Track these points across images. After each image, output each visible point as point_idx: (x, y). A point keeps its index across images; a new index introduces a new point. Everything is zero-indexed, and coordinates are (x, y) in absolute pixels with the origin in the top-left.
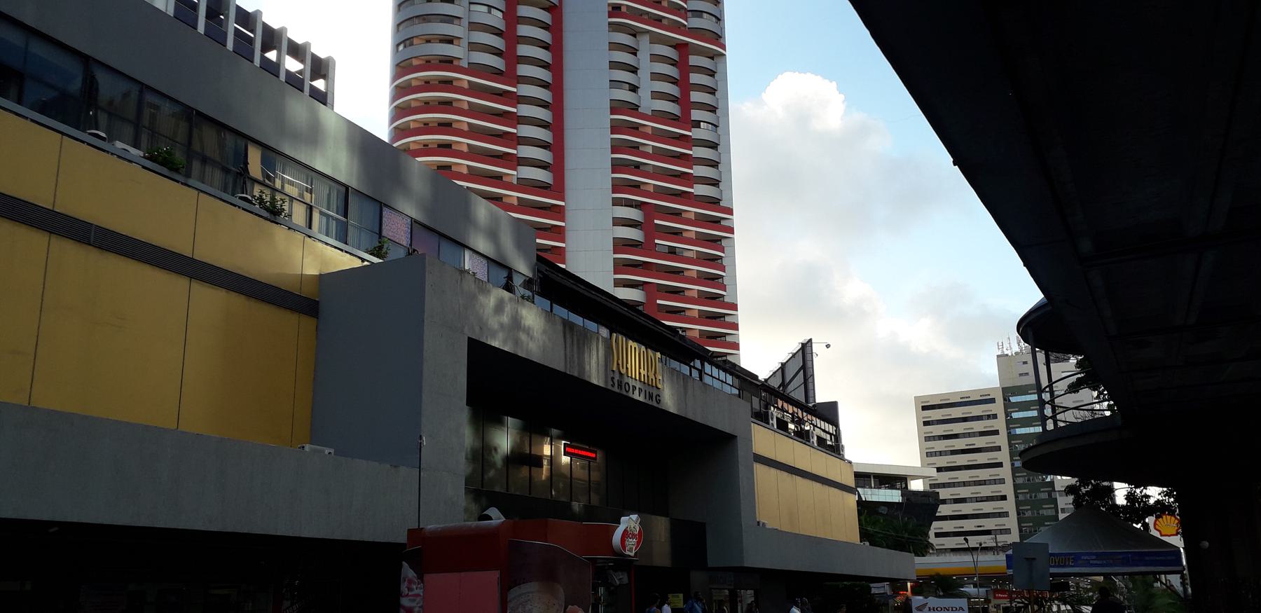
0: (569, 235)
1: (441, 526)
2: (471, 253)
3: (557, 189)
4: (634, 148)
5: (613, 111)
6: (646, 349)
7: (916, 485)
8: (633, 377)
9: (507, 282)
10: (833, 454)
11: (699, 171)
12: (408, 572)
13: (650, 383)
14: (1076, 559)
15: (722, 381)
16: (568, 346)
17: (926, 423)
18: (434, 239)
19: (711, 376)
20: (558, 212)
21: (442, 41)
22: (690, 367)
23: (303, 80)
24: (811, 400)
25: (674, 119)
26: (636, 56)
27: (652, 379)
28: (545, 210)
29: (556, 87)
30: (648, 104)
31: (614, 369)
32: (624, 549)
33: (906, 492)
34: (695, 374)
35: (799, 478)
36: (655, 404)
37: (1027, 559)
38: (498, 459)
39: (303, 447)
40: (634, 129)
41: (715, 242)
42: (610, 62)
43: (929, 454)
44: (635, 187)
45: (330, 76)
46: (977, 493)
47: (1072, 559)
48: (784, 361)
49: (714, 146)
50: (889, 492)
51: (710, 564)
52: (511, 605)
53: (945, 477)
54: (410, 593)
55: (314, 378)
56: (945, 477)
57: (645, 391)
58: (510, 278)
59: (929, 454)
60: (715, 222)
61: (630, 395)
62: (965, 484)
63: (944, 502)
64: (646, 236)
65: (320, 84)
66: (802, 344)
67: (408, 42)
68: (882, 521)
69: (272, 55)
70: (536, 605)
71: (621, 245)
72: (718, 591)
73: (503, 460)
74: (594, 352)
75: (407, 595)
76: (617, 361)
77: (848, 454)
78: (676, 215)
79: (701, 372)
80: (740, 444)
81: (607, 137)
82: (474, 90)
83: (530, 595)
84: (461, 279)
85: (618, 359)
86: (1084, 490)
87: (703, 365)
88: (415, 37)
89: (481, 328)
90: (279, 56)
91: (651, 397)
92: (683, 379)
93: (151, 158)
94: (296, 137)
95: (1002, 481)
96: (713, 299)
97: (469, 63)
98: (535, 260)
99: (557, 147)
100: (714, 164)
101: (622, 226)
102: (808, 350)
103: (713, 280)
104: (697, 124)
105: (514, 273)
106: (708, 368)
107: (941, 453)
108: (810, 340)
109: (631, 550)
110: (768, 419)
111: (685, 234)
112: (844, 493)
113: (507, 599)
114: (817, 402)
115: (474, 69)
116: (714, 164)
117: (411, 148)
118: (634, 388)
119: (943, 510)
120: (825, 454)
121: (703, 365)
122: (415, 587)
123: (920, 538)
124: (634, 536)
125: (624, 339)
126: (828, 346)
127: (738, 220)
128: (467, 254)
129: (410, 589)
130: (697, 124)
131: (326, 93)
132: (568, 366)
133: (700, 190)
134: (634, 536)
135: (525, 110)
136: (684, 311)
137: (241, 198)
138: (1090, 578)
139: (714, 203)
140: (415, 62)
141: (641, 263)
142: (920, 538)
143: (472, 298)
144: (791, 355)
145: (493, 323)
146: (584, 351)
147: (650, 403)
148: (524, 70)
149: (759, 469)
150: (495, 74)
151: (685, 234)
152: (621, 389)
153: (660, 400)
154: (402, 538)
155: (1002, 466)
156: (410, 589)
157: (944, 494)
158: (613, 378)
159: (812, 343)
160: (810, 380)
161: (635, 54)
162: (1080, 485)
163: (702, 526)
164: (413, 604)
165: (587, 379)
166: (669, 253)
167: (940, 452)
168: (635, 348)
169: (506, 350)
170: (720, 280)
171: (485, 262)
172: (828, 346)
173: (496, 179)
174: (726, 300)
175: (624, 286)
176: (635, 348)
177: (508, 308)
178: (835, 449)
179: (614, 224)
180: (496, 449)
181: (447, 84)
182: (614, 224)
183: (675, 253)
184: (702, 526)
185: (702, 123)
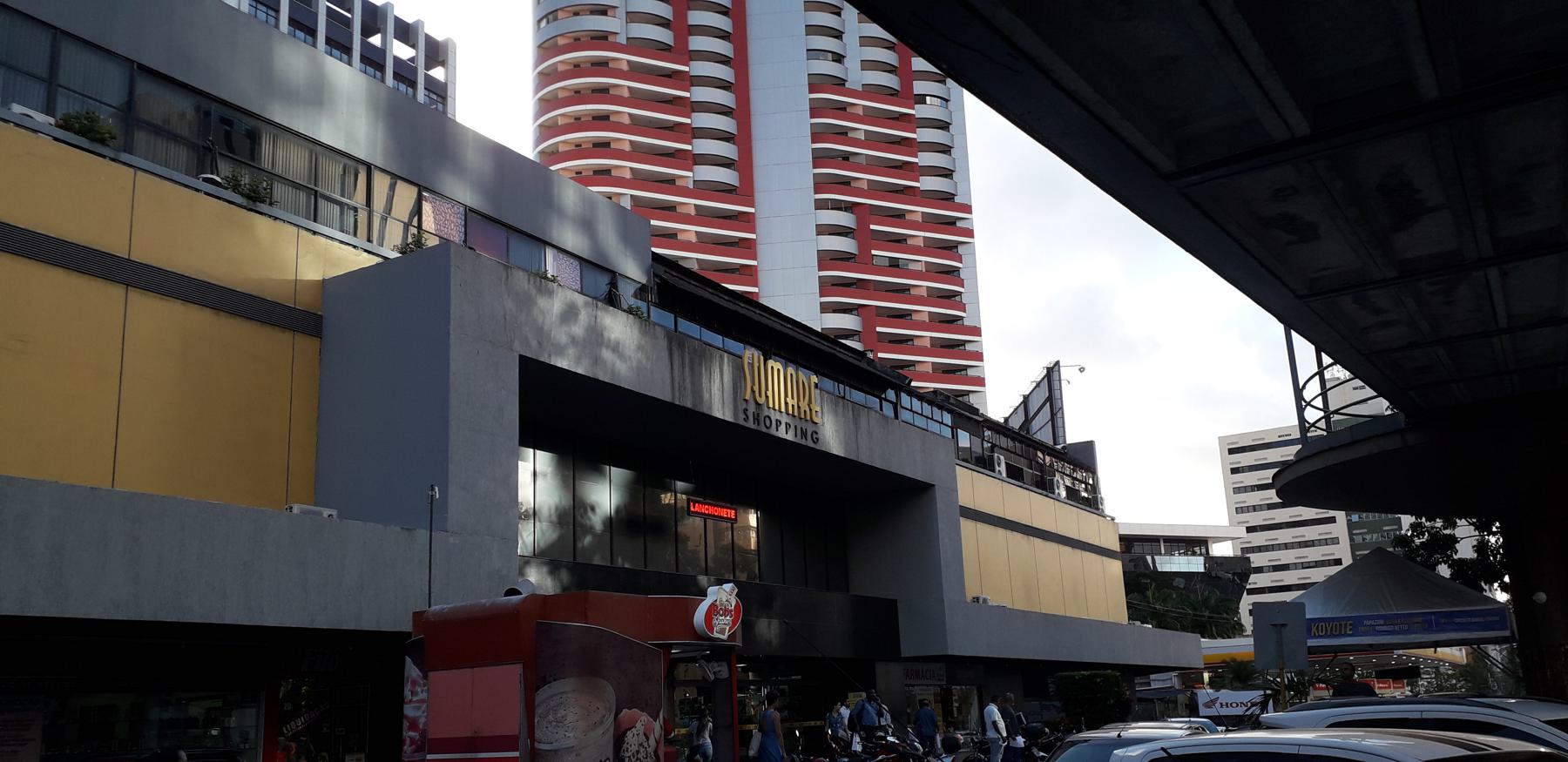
0: (762, 250)
1: (449, 606)
2: (556, 251)
3: (744, 191)
4: (841, 134)
5: (812, 89)
6: (797, 370)
7: (1221, 550)
8: (777, 408)
9: (610, 290)
10: (1088, 509)
11: (926, 159)
12: (412, 670)
13: (803, 416)
14: (1356, 625)
15: (927, 417)
16: (676, 367)
17: (1234, 471)
18: (501, 234)
19: (911, 410)
20: (746, 221)
21: (593, 13)
22: (881, 399)
23: (416, 68)
24: (1061, 440)
25: (892, 95)
26: (840, 16)
27: (805, 411)
28: (730, 219)
29: (739, 62)
30: (857, 77)
31: (747, 398)
32: (711, 630)
33: (1210, 560)
34: (888, 410)
35: (1038, 541)
36: (810, 444)
37: (1275, 625)
38: (597, 521)
39: (291, 508)
40: (841, 110)
41: (950, 249)
42: (806, 26)
43: (1240, 510)
44: (844, 185)
45: (449, 62)
46: (1303, 557)
47: (1350, 625)
48: (1027, 393)
49: (944, 126)
50: (1184, 559)
51: (907, 650)
52: (539, 711)
53: (1260, 539)
54: (414, 699)
55: (318, 417)
56: (1260, 539)
57: (796, 427)
58: (613, 285)
59: (1240, 510)
60: (950, 224)
61: (773, 431)
62: (1286, 546)
63: (1259, 570)
64: (860, 247)
65: (438, 73)
66: (1047, 368)
67: (551, 17)
68: (1174, 596)
69: (376, 40)
70: (571, 709)
71: (828, 259)
72: (925, 688)
73: (604, 524)
74: (717, 376)
75: (411, 701)
76: (766, 393)
77: (1109, 507)
78: (898, 217)
79: (896, 406)
80: (939, 494)
81: (806, 122)
82: (636, 72)
83: (564, 696)
84: (507, 278)
85: (767, 389)
86: (1417, 541)
87: (898, 396)
88: (560, 9)
89: (539, 343)
90: (384, 40)
91: (804, 434)
92: (853, 411)
93: (65, 125)
94: (291, 96)
95: (1335, 541)
96: (950, 322)
97: (628, 38)
98: (649, 260)
99: (742, 138)
100: (946, 149)
101: (830, 234)
102: (1055, 374)
103: (949, 298)
104: (921, 99)
105: (619, 278)
106: (905, 399)
107: (1255, 508)
108: (1057, 363)
109: (722, 631)
110: (994, 466)
111: (910, 242)
112: (1104, 558)
113: (534, 701)
114: (1069, 441)
115: (636, 45)
116: (946, 149)
117: (560, 150)
118: (779, 422)
119: (1256, 580)
120: (1075, 508)
121: (898, 396)
122: (419, 690)
123: (1225, 615)
124: (726, 612)
125: (762, 358)
126: (1082, 370)
127: (979, 220)
128: (550, 253)
129: (413, 693)
130: (921, 99)
131: (446, 84)
132: (677, 394)
133: (928, 183)
134: (726, 612)
135: (701, 94)
136: (912, 340)
137: (206, 180)
138: (1395, 651)
139: (947, 199)
140: (561, 41)
141: (737, 240)
142: (1225, 615)
143: (526, 303)
144: (1034, 384)
145: (561, 335)
146: (701, 374)
147: (803, 442)
148: (698, 43)
149: (967, 527)
150: (662, 50)
151: (910, 242)
152: (758, 424)
153: (817, 439)
154: (406, 626)
155: (1335, 522)
156: (413, 693)
157: (1257, 560)
158: (745, 411)
159: (1059, 367)
160: (1059, 415)
161: (839, 14)
162: (1412, 535)
163: (892, 605)
164: (419, 713)
165: (705, 411)
166: (890, 266)
167: (1254, 506)
168: (778, 370)
169: (580, 371)
170: (958, 298)
171: (576, 263)
172: (1082, 370)
173: (668, 183)
174: (967, 322)
175: (835, 311)
176: (778, 370)
177: (584, 317)
178: (1091, 502)
179: (819, 234)
180: (593, 509)
181: (601, 66)
182: (819, 234)
183: (898, 266)
184: (892, 605)
185: (928, 98)
